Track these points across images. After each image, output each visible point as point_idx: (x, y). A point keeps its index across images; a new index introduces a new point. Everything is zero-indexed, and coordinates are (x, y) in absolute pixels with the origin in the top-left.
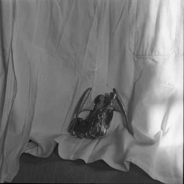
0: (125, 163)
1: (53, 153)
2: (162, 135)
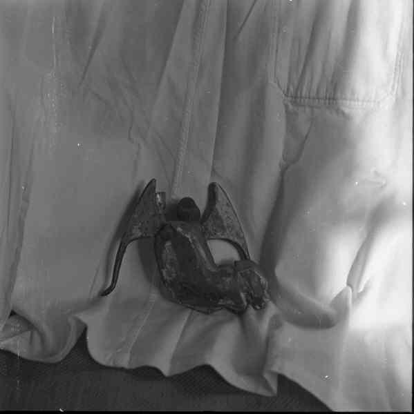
0: (267, 376)
1: (74, 349)
2: (350, 302)
